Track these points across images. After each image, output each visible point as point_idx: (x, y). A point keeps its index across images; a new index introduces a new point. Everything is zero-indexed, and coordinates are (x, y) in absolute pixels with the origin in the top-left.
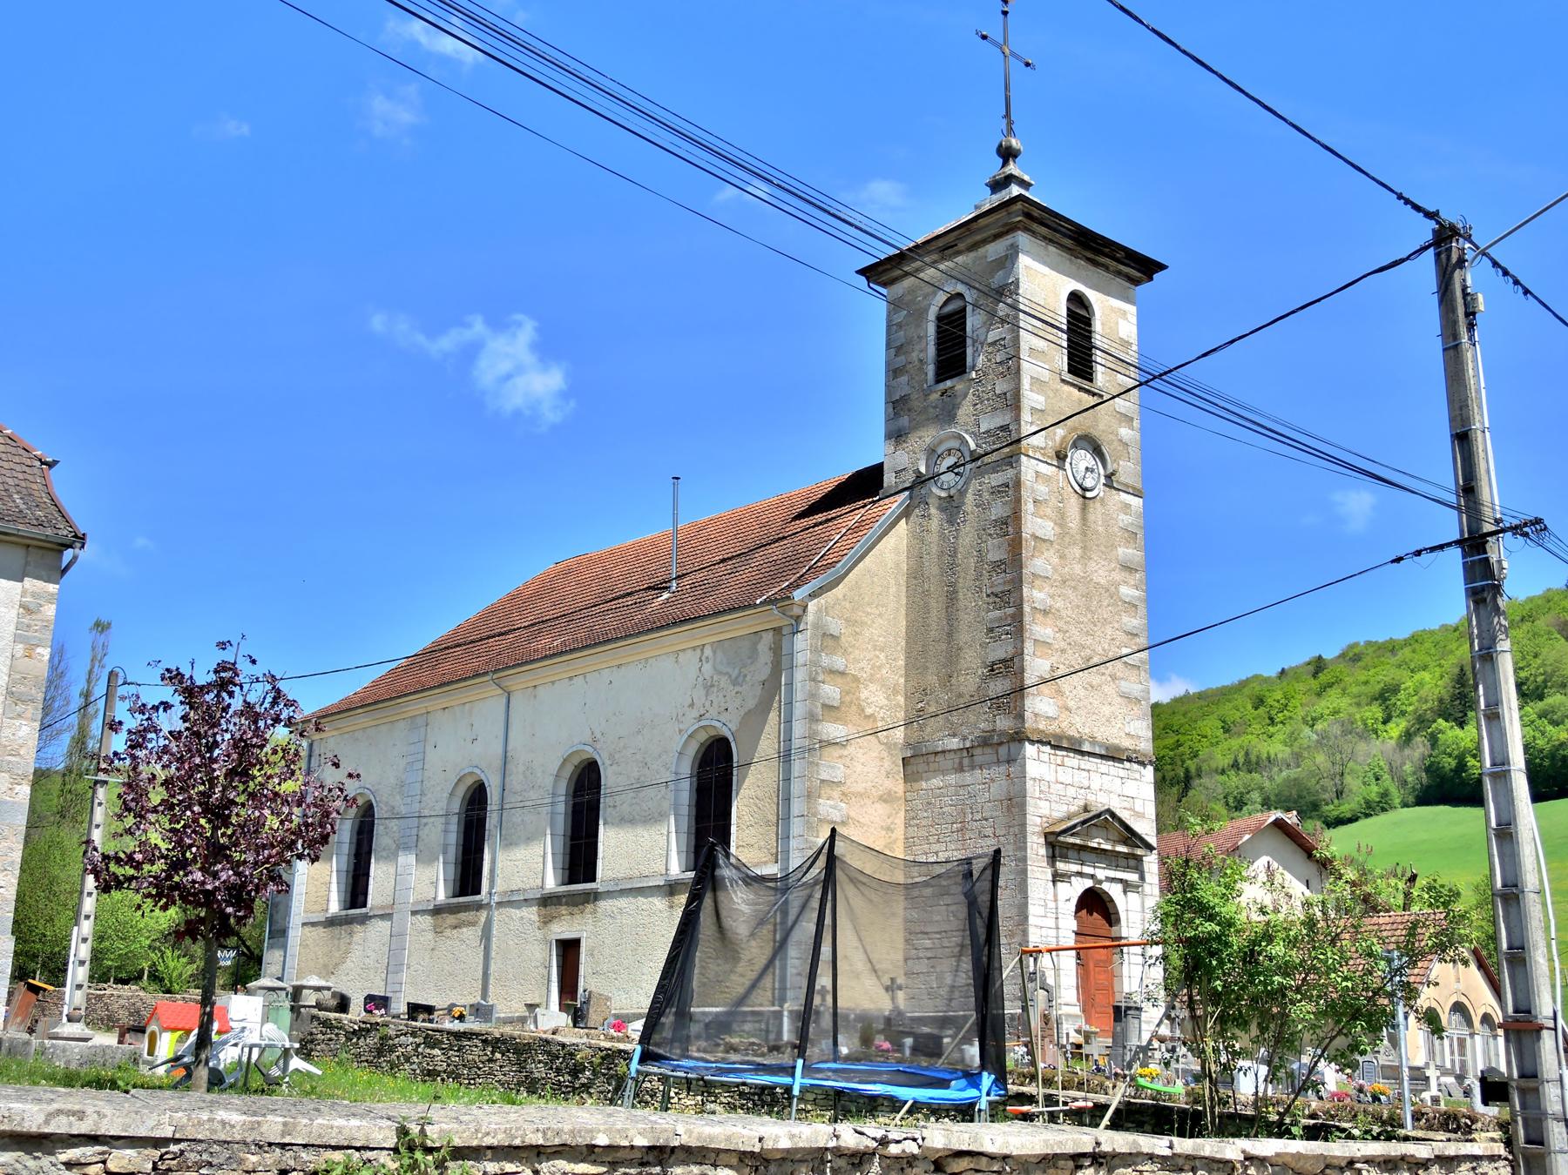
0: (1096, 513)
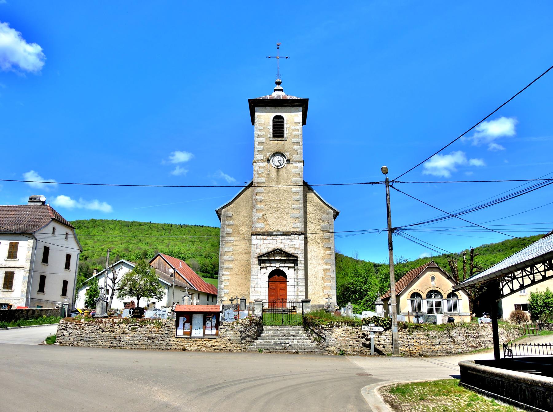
0: (283, 172)
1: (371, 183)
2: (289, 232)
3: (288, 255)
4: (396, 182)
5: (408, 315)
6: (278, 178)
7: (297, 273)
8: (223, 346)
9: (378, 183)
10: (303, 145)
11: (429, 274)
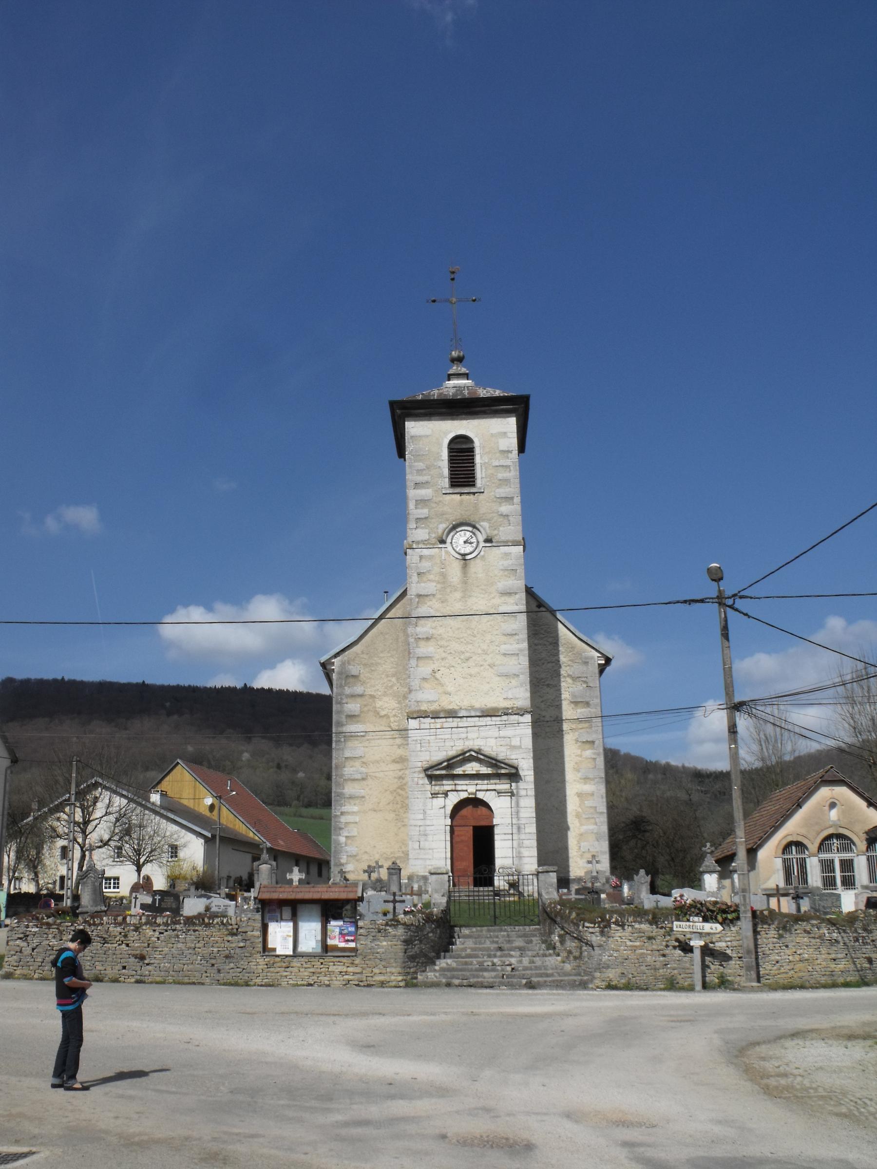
0: (476, 567)
1: (685, 602)
2: (496, 709)
3: (493, 762)
4: (741, 597)
5: (778, 893)
6: (465, 583)
7: (518, 805)
8: (367, 972)
9: (702, 601)
10: (523, 502)
11: (825, 793)
